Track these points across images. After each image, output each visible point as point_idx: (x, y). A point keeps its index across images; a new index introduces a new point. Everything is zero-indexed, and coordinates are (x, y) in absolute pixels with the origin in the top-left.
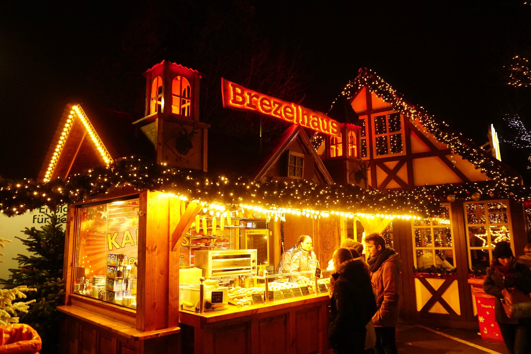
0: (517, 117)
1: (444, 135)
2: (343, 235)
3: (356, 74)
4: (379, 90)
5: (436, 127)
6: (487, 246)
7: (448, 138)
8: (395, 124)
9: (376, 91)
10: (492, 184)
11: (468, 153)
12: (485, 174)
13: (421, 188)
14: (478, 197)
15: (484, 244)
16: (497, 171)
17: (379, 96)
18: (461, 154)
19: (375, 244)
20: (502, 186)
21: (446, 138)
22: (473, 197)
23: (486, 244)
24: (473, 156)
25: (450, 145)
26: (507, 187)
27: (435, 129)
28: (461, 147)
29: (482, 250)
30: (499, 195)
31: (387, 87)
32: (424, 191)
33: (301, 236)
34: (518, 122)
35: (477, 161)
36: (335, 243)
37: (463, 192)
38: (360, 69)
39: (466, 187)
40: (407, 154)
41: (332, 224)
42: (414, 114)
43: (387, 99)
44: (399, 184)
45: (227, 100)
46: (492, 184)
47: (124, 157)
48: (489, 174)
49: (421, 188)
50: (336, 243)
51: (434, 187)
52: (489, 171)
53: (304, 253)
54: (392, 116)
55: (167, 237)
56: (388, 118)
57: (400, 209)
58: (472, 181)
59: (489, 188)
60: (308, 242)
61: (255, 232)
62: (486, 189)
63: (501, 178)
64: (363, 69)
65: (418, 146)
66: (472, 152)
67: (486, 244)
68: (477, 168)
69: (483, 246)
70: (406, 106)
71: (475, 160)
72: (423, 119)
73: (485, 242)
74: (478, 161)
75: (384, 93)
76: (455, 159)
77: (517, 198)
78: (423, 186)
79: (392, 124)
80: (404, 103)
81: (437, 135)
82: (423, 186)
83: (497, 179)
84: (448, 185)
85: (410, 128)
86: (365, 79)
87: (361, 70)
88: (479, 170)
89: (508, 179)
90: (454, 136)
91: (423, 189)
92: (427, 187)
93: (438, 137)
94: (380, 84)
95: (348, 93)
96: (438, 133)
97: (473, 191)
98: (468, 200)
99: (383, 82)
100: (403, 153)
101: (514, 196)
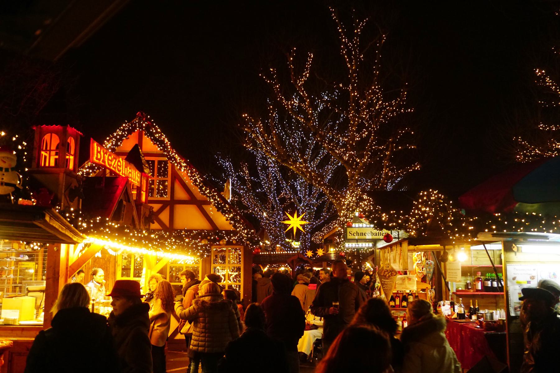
0: (229, 159)
1: (206, 190)
2: (119, 271)
3: (135, 117)
4: (155, 138)
5: (201, 182)
6: (225, 282)
7: (210, 193)
8: (161, 170)
9: (152, 138)
10: (235, 233)
11: (222, 207)
12: (232, 225)
13: (181, 231)
14: (225, 243)
15: (222, 281)
16: (241, 224)
17: (154, 144)
18: (217, 207)
19: (186, 278)
20: (242, 235)
21: (208, 193)
22: (221, 243)
23: (224, 280)
24: (226, 210)
25: (210, 199)
26: (246, 237)
27: (200, 183)
28: (218, 201)
29: (221, 285)
30: (240, 242)
31: (163, 137)
32: (183, 234)
33: (93, 270)
34: (229, 164)
35: (228, 214)
36: (109, 278)
37: (214, 238)
38: (138, 113)
39: (217, 234)
40: (171, 199)
41: (106, 259)
42: (185, 167)
43: (161, 148)
44: (161, 227)
45: (93, 156)
46: (235, 233)
47: (262, 254)
48: (235, 226)
49: (181, 231)
50: (110, 277)
51: (191, 231)
52: (235, 224)
53: (97, 285)
54: (160, 162)
55: (65, 267)
56: (156, 163)
57: (118, 240)
58: (220, 229)
59: (232, 237)
60: (101, 275)
61: (26, 265)
62: (231, 237)
63: (243, 229)
64: (142, 114)
65: (180, 194)
66: (225, 207)
67: (224, 280)
68: (227, 220)
69: (222, 282)
70: (179, 158)
71: (226, 213)
72: (191, 173)
73: (223, 279)
74: (229, 215)
75: (156, 141)
76: (211, 210)
77: (251, 246)
78: (183, 230)
79: (159, 169)
80: (177, 155)
81: (201, 188)
82: (183, 230)
83: (240, 230)
84: (202, 231)
85: (176, 177)
86: (144, 125)
87: (139, 113)
88: (228, 222)
89: (248, 231)
90: (214, 192)
91: (182, 232)
92: (186, 231)
93: (202, 190)
94: (157, 132)
95: (125, 134)
96: (202, 187)
97: (221, 238)
98: (217, 245)
99: (159, 132)
100: (167, 198)
101: (249, 244)
